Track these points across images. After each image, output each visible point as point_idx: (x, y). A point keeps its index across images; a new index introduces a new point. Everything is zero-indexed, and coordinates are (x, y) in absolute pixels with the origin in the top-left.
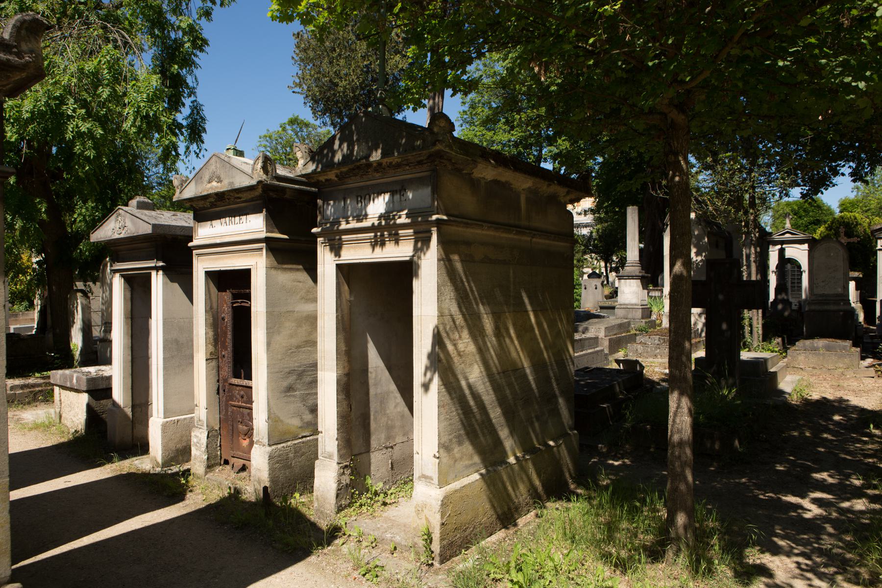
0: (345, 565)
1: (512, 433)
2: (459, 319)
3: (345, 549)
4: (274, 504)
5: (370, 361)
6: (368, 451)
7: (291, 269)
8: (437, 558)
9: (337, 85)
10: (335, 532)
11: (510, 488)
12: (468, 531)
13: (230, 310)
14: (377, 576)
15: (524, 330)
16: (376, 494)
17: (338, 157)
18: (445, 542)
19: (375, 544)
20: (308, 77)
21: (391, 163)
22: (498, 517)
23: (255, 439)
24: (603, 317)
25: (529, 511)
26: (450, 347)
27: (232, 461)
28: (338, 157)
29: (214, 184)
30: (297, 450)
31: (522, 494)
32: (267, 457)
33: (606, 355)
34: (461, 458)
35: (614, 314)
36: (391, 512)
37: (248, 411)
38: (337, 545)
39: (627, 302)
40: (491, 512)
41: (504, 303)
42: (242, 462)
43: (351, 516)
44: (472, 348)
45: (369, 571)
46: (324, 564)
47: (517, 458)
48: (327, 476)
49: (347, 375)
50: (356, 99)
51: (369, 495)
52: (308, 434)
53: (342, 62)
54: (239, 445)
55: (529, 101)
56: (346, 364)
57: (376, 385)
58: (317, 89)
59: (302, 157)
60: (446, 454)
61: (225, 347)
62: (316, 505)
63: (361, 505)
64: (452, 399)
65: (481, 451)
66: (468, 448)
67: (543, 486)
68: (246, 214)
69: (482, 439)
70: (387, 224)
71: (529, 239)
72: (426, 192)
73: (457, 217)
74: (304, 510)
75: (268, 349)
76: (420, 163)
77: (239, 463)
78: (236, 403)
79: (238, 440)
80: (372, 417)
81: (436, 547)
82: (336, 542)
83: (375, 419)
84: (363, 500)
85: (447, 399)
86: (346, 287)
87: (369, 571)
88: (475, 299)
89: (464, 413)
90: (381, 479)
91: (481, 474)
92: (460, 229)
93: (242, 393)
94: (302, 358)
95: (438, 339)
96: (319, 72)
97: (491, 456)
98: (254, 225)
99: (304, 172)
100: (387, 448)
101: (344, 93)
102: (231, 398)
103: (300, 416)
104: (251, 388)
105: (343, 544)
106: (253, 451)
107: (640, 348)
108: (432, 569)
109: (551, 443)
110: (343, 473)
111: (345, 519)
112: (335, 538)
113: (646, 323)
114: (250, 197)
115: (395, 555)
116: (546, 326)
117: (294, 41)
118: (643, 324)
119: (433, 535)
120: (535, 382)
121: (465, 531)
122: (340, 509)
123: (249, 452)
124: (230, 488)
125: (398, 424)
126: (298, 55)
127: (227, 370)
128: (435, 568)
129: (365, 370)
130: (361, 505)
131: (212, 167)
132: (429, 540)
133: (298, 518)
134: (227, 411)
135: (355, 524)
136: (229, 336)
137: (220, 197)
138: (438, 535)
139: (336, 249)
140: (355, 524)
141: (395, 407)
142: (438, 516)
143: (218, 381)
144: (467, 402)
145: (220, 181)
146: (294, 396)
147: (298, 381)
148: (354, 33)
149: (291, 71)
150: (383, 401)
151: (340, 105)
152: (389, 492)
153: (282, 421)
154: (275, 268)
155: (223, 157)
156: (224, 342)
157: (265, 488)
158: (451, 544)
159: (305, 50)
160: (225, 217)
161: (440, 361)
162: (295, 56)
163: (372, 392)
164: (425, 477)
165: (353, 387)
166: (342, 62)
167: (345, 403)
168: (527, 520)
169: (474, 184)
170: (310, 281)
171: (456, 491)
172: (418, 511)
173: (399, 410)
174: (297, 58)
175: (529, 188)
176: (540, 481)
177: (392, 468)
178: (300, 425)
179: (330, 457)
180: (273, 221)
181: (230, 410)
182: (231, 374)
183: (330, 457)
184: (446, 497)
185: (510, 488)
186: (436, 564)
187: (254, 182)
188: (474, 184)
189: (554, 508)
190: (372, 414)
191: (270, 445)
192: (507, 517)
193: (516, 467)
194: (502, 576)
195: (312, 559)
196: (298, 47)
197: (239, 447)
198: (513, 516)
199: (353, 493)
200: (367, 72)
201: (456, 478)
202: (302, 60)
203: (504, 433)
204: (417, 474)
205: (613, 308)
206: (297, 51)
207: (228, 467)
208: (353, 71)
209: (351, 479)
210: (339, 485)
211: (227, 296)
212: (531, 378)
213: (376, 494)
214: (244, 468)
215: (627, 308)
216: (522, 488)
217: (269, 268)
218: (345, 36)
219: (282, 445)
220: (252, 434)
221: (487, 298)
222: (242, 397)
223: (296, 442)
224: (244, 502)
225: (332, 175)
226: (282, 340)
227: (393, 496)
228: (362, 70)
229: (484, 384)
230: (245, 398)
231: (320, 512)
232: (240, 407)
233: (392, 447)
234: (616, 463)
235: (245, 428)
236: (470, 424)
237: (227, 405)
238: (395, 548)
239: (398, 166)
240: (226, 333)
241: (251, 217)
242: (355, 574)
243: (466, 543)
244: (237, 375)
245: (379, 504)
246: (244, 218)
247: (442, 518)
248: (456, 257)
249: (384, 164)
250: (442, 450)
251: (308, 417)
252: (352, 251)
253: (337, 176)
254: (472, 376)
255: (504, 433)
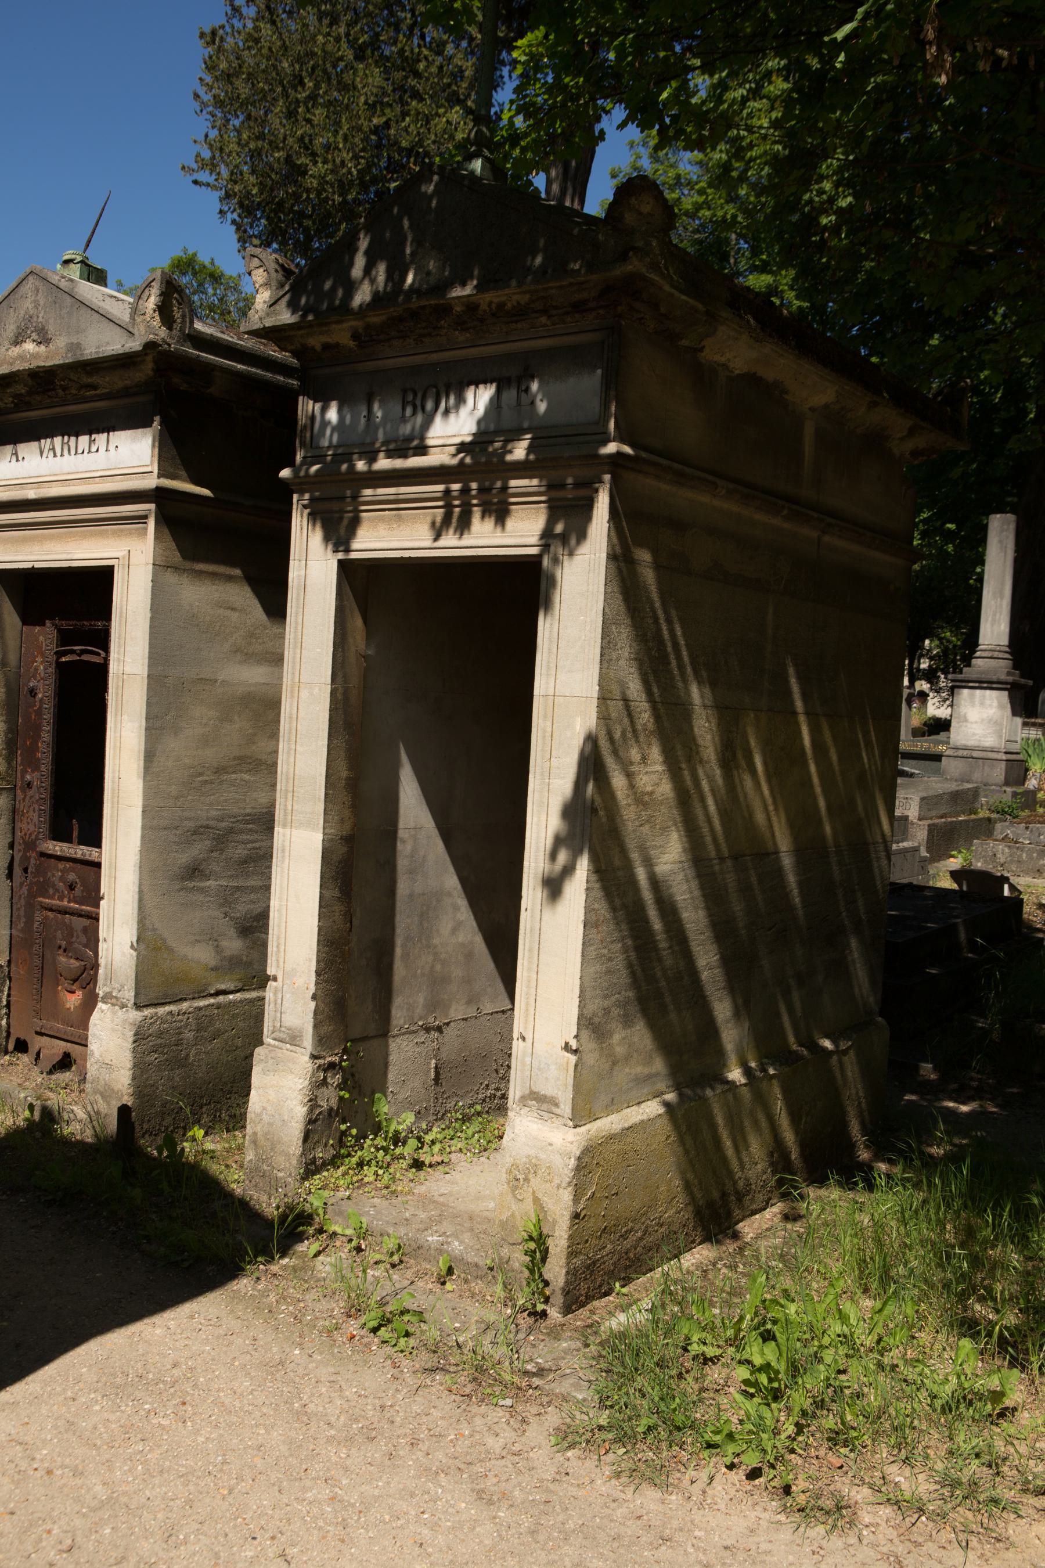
0: (324, 1305)
1: (737, 1014)
2: (645, 717)
3: (324, 1266)
4: (141, 1153)
5: (402, 811)
6: (383, 1032)
7: (214, 575)
8: (558, 1299)
9: (303, 171)
10: (293, 1228)
11: (728, 1143)
12: (633, 1238)
13: (51, 670)
14: (407, 1334)
15: (785, 762)
16: (397, 1140)
17: (362, 296)
18: (578, 1262)
19: (398, 1258)
20: (233, 146)
21: (501, 306)
22: (698, 1213)
23: (101, 991)
24: (911, 775)
25: (767, 1204)
26: (618, 781)
27: (37, 1043)
28: (362, 296)
29: (29, 346)
30: (202, 1021)
31: (753, 1162)
32: (130, 1035)
33: (924, 860)
34: (627, 1058)
35: (938, 772)
36: (433, 1184)
37: (86, 922)
38: (304, 1255)
39: (971, 742)
40: (681, 1199)
41: (746, 685)
42: (61, 1046)
43: (337, 1188)
44: (666, 788)
45: (385, 1321)
46: (273, 1298)
47: (747, 1072)
48: (282, 1090)
49: (348, 840)
50: (348, 211)
51: (380, 1142)
52: (231, 986)
53: (319, 114)
54: (57, 1004)
55: (755, 251)
56: (347, 813)
57: (412, 871)
58: (253, 179)
59: (267, 285)
60: (592, 1045)
61: (32, 763)
62: (250, 1156)
63: (361, 1164)
64: (613, 909)
65: (669, 1045)
66: (641, 1035)
67: (803, 1145)
68: (108, 429)
69: (673, 1016)
70: (476, 463)
71: (815, 534)
72: (591, 382)
73: (653, 454)
74: (215, 1168)
75: (147, 769)
76: (578, 308)
77: (54, 1049)
78: (56, 902)
79: (56, 994)
80: (398, 951)
81: (556, 1271)
82: (301, 1247)
83: (406, 956)
84: (367, 1152)
85: (602, 908)
86: (359, 622)
87: (385, 1321)
88: (681, 667)
89: (637, 948)
90: (410, 1105)
91: (667, 1104)
92: (665, 487)
93: (72, 877)
94: (232, 799)
95: (592, 765)
96: (261, 137)
97: (691, 1065)
98: (129, 456)
99: (269, 323)
100: (428, 1030)
101: (319, 194)
102: (43, 888)
103: (214, 939)
104: (98, 865)
105: (318, 1254)
106: (95, 1018)
107: (1003, 852)
108: (543, 1324)
109: (827, 1044)
110: (324, 1083)
111: (326, 1193)
112: (300, 1238)
113: (1015, 794)
114: (120, 384)
115: (449, 1286)
116: (834, 757)
117: (201, 51)
118: (1007, 798)
119: (550, 1242)
120: (801, 892)
121: (624, 1237)
122: (311, 1169)
123: (84, 1022)
124: (31, 1107)
125: (457, 972)
126: (211, 88)
127: (35, 818)
128: (548, 1322)
129: (389, 833)
130: (361, 1164)
131: (26, 305)
132: (538, 1248)
133: (207, 1191)
134: (30, 920)
135: (350, 1208)
136: (47, 734)
137: (43, 381)
138: (564, 1243)
139: (339, 530)
140: (350, 1208)
141: (454, 930)
142: (567, 1196)
143: (11, 846)
144: (646, 920)
145: (44, 339)
146: (202, 890)
147: (218, 853)
148: (352, 43)
149: (190, 129)
150: (429, 908)
151: (308, 223)
152: (428, 1138)
153: (170, 950)
154: (176, 569)
155: (55, 279)
156: (32, 750)
157: (124, 1111)
158: (591, 1267)
159: (228, 77)
160: (52, 436)
161: (590, 820)
162: (201, 91)
163: (403, 887)
164: (538, 1100)
165: (359, 871)
166: (319, 114)
167: (338, 908)
168: (762, 1226)
169: (702, 377)
170: (258, 612)
171: (612, 1137)
172: (516, 1182)
173: (461, 939)
174: (207, 97)
175: (826, 406)
176: (797, 1133)
177: (437, 1080)
178: (213, 963)
179: (293, 1039)
180: (174, 451)
181: (38, 917)
182: (45, 829)
183: (293, 1039)
184: (587, 1151)
185: (728, 1143)
186: (555, 1314)
187: (135, 345)
188: (702, 377)
189: (826, 1201)
190: (399, 942)
191: (138, 1006)
192: (715, 1217)
193: (746, 1094)
194: (718, 1352)
195: (242, 1285)
196: (211, 67)
197: (56, 1010)
198: (729, 1214)
199: (344, 1134)
200: (379, 146)
201: (613, 1106)
202: (219, 103)
203: (722, 1009)
204: (515, 1091)
205: (937, 758)
206: (208, 79)
207: (25, 1059)
208: (345, 139)
209: (341, 1098)
210: (311, 1110)
211: (46, 636)
212: (792, 879)
213: (397, 1140)
214: (65, 1063)
215: (973, 756)
216: (757, 1148)
217: (160, 567)
218: (329, 48)
219: (168, 1008)
220: (94, 979)
221: (712, 673)
222: (71, 887)
223: (202, 1003)
224: (67, 1143)
225: (341, 335)
226: (179, 748)
227: (436, 1148)
228: (366, 139)
229: (687, 881)
230: (78, 891)
231: (257, 1173)
232: (64, 912)
233: (439, 1029)
234: (964, 1108)
235: (74, 963)
236: (648, 981)
237: (30, 907)
238: (450, 1271)
239: (520, 313)
240: (37, 729)
241: (120, 438)
242: (353, 1326)
243: (631, 1266)
244: (59, 834)
245: (404, 1164)
246: (101, 438)
247: (576, 1200)
248: (644, 556)
249: (484, 307)
250: (585, 1034)
251: (234, 945)
252: (382, 530)
253: (355, 336)
254: (666, 858)
255: (722, 1009)
